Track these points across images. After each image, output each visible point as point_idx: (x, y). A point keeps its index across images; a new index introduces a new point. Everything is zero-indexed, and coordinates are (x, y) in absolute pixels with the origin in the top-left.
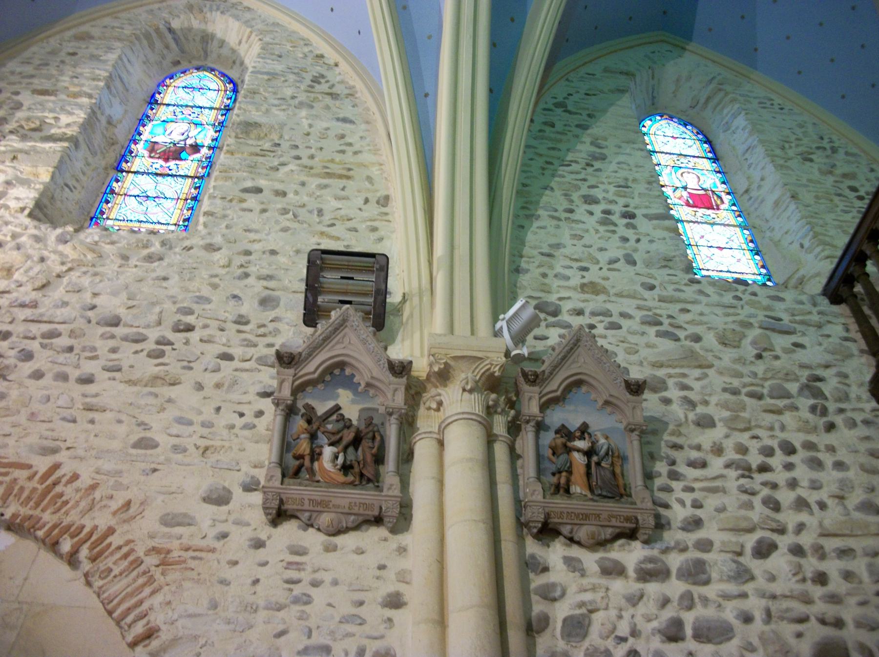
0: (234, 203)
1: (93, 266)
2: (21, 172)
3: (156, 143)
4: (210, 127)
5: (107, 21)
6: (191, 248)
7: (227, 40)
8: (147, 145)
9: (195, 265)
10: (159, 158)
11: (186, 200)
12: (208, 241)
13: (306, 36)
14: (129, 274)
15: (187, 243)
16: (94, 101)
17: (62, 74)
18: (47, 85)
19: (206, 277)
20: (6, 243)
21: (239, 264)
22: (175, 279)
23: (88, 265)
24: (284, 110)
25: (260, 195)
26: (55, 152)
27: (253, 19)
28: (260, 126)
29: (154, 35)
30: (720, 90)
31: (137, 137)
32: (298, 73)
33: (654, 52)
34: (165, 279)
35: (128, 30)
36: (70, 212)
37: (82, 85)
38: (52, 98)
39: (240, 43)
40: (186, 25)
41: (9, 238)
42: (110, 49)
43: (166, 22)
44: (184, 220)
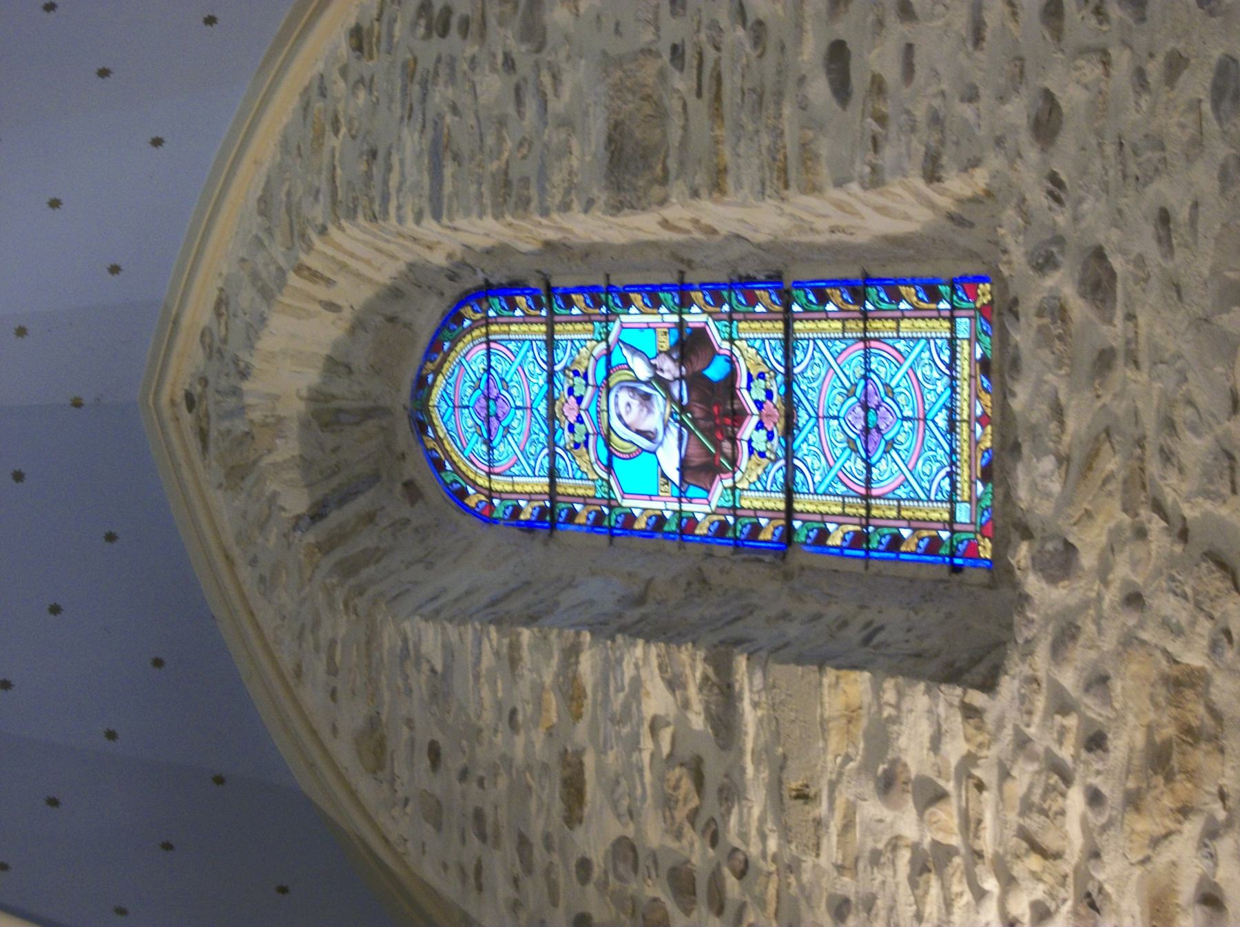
0: (886, 108)
1: (1140, 443)
2: (848, 759)
3: (684, 467)
4: (615, 327)
5: (313, 696)
6: (1054, 179)
7: (326, 351)
8: (693, 492)
9: (1110, 149)
10: (733, 440)
11: (865, 315)
12: (1024, 137)
13: (295, 102)
14: (1158, 330)
15: (1038, 198)
16: (586, 637)
17: (508, 761)
18: (550, 793)
19: (1145, 101)
20: (1085, 721)
21: (1093, 22)
22: (1166, 191)
23: (1141, 459)
24: (556, 78)
25: (852, 46)
26: (768, 687)
27: (255, 277)
28: (617, 125)
29: (338, 554)
31: (671, 527)
32: (424, 85)
34: (1165, 218)
35: (339, 626)
36: (949, 615)
37: (538, 690)
38: (589, 760)
39: (332, 306)
40: (295, 474)
41: (1072, 721)
42: (408, 654)
43: (295, 527)
44: (935, 297)
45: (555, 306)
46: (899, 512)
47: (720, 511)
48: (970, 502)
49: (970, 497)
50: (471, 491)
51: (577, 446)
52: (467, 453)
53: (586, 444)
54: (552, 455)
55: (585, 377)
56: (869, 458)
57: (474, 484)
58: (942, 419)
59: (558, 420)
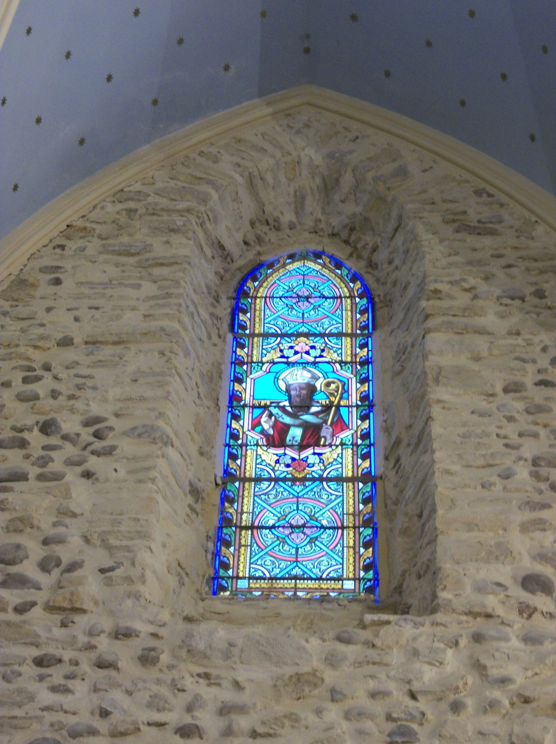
44: (366, 569)
45: (361, 338)
46: (244, 546)
47: (245, 436)
48: (249, 588)
49: (252, 588)
50: (256, 284)
51: (281, 351)
52: (277, 282)
54: (276, 335)
55: (321, 356)
56: (284, 297)
57: (260, 286)
58: (297, 571)
59: (296, 339)
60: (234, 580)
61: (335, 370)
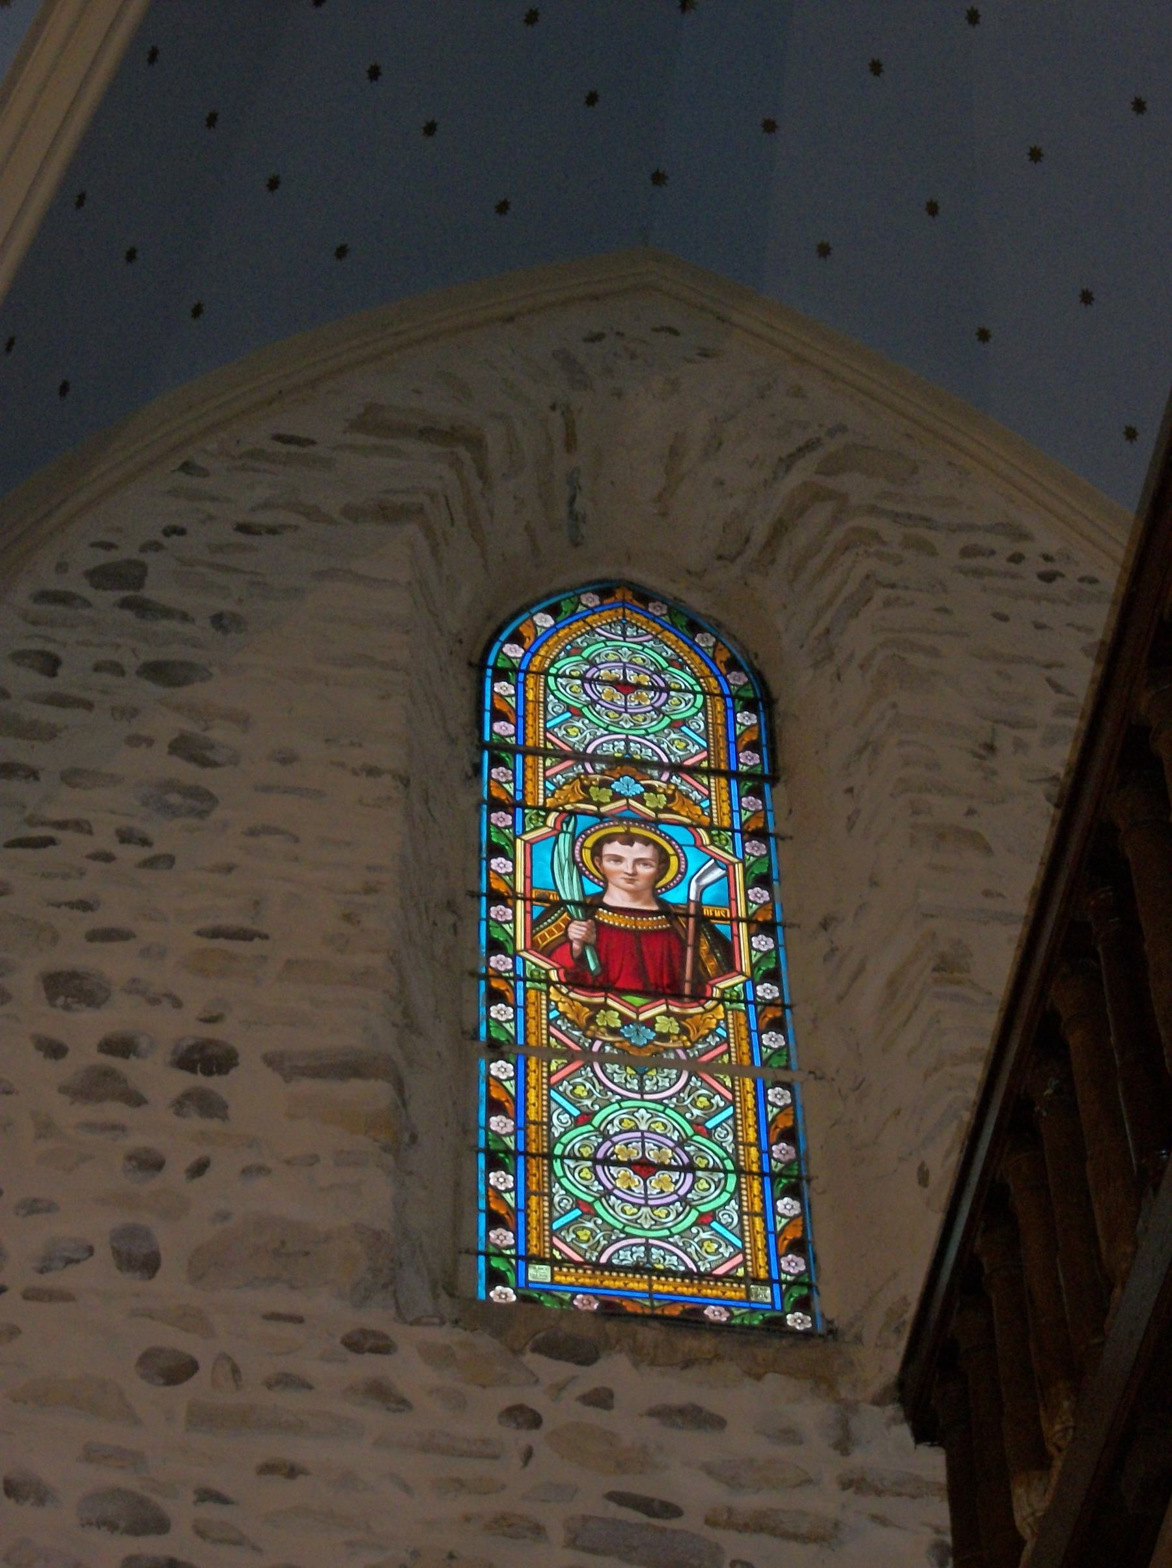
30: (820, 495)
33: (596, 338)
49: (559, 1283)
51: (585, 788)
53: (588, 800)
60: (522, 1264)
61: (699, 843)
